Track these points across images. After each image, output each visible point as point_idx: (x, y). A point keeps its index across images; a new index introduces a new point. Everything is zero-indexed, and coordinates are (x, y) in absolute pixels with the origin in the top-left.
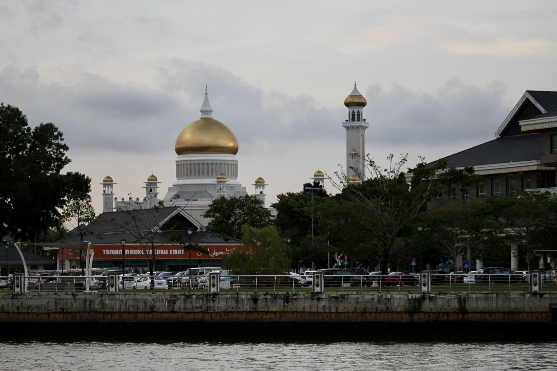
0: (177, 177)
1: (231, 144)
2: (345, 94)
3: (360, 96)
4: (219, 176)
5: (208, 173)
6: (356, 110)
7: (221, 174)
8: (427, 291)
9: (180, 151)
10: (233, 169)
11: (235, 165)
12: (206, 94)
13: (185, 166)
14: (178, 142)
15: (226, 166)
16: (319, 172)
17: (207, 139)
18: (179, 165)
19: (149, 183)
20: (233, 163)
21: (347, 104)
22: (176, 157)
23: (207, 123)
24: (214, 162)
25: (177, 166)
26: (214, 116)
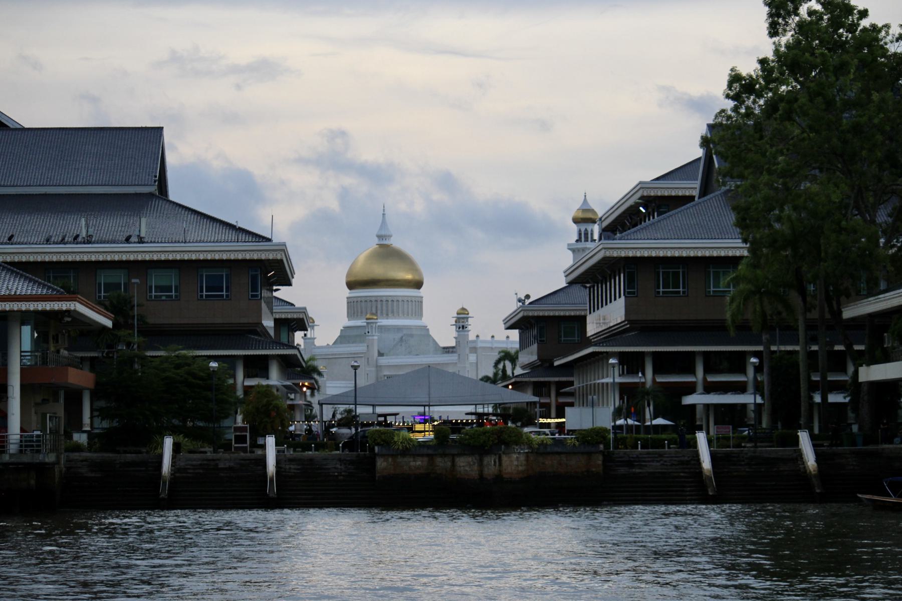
0: (348, 316)
1: (409, 277)
2: (574, 209)
3: (593, 211)
4: (368, 316)
5: (382, 312)
6: (583, 227)
7: (372, 314)
8: (457, 459)
9: (351, 285)
10: (417, 308)
11: (419, 302)
12: (384, 214)
13: (363, 304)
14: (348, 275)
15: (395, 303)
16: (463, 309)
17: (379, 271)
18: (351, 302)
19: (458, 318)
20: (417, 299)
21: (576, 221)
22: (347, 292)
23: (387, 252)
24: (379, 299)
25: (348, 303)
26: (396, 242)
